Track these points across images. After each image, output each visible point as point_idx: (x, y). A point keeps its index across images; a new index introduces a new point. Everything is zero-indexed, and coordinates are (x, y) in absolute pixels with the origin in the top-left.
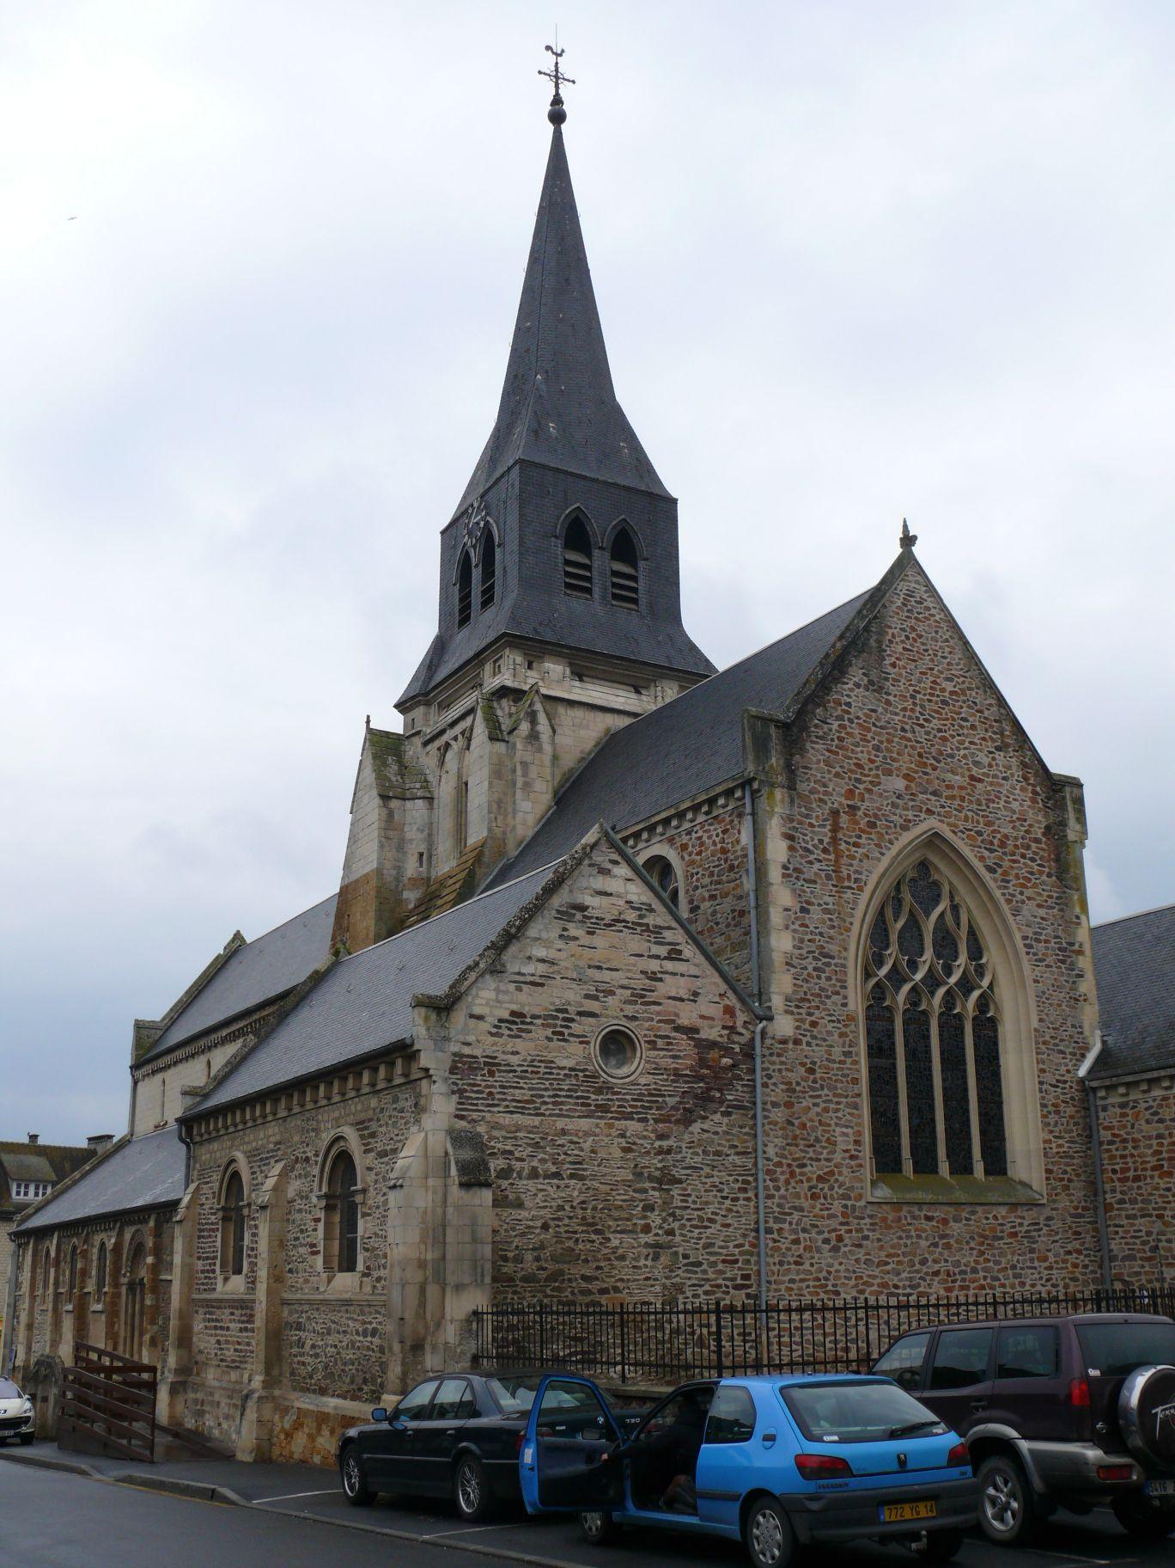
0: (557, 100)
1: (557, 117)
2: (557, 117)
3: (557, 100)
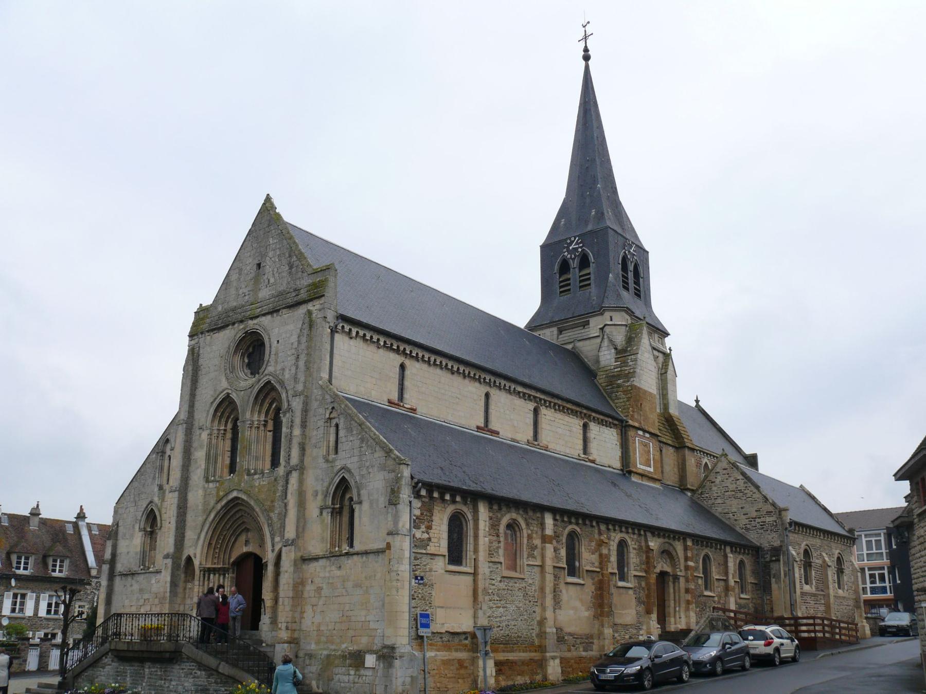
0: (586, 50)
1: (587, 58)
2: (587, 58)
3: (586, 50)
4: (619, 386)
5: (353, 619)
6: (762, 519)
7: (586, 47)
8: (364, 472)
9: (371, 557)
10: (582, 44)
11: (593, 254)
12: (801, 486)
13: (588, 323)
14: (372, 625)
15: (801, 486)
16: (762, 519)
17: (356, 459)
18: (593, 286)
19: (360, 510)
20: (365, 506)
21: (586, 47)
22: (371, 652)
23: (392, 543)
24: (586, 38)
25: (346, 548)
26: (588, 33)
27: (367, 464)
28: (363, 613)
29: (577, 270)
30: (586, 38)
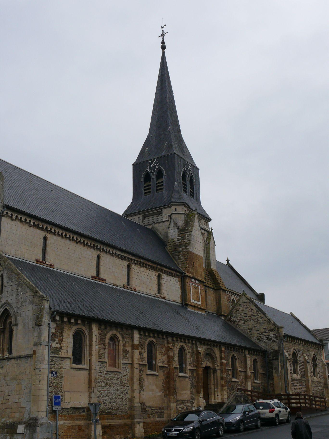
0: (163, 43)
1: (163, 47)
2: (163, 47)
3: (163, 43)
4: (180, 251)
5: (10, 401)
6: (267, 334)
7: (163, 40)
8: (20, 305)
9: (23, 360)
10: (161, 39)
11: (165, 167)
12: (291, 313)
13: (161, 212)
14: (23, 405)
15: (291, 313)
16: (267, 334)
17: (14, 297)
18: (165, 189)
19: (17, 330)
20: (20, 327)
21: (163, 40)
22: (21, 423)
23: (37, 351)
24: (163, 35)
25: (7, 355)
26: (165, 32)
27: (22, 300)
28: (17, 397)
29: (155, 180)
30: (163, 35)
